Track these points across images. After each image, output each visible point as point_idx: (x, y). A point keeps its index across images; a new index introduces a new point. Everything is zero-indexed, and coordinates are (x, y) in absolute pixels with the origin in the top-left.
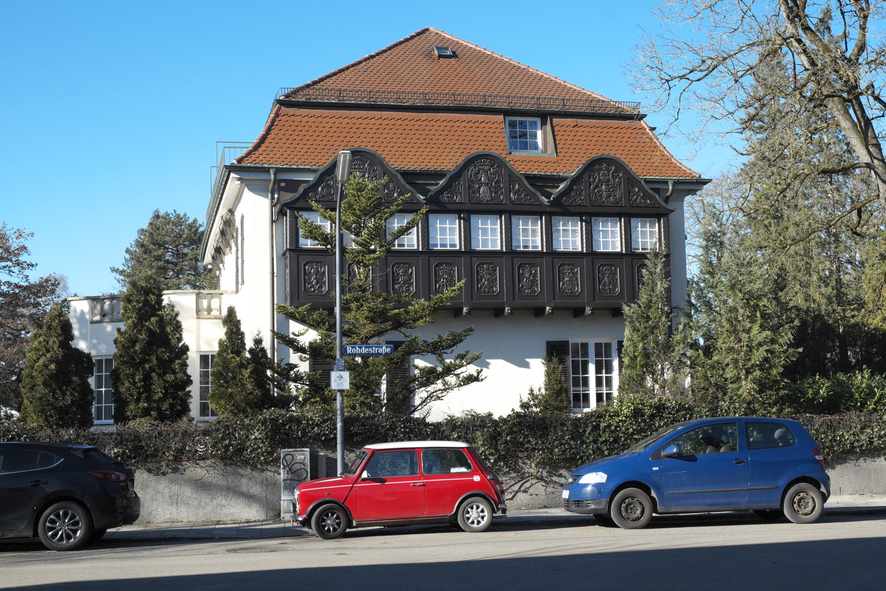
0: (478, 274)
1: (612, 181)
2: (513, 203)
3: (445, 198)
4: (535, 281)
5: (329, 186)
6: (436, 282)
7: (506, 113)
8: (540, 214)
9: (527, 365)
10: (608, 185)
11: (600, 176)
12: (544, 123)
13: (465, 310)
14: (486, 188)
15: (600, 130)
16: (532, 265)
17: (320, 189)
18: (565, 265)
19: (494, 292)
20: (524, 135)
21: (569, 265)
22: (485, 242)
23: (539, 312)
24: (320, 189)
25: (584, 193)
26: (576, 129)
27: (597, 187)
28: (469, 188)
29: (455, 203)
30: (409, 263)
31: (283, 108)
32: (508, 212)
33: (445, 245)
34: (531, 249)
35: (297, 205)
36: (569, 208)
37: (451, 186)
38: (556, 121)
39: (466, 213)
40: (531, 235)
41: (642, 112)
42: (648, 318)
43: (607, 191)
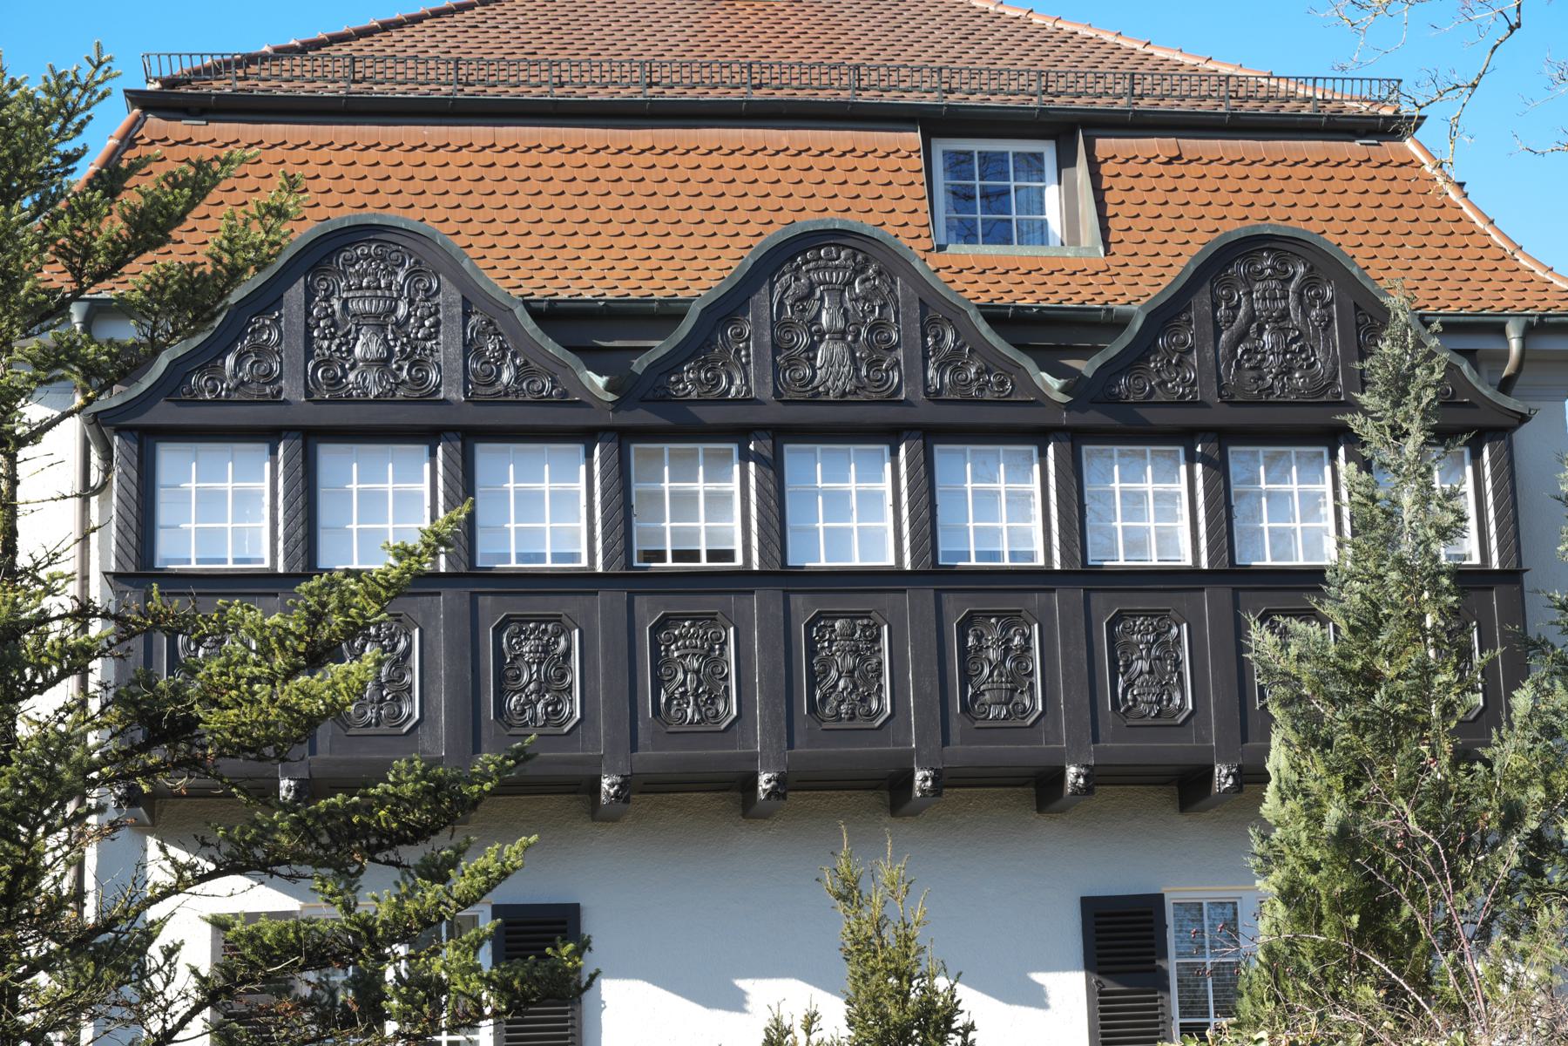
0: (812, 651)
1: (1295, 316)
2: (936, 398)
3: (688, 382)
4: (1030, 673)
5: (261, 350)
6: (658, 684)
7: (935, 123)
8: (1037, 436)
9: (1036, 998)
10: (1285, 331)
11: (1251, 299)
12: (1066, 160)
13: (764, 781)
14: (838, 348)
15: (1260, 170)
16: (1011, 619)
17: (230, 361)
18: (1134, 614)
19: (871, 716)
20: (995, 198)
21: (1147, 614)
22: (838, 538)
23: (1044, 788)
24: (230, 361)
25: (1194, 358)
26: (1176, 169)
27: (1242, 336)
28: (776, 349)
29: (723, 400)
30: (556, 619)
31: (152, 120)
32: (920, 431)
33: (694, 555)
34: (1006, 562)
35: (147, 419)
36: (1144, 412)
37: (709, 343)
38: (1105, 146)
39: (770, 436)
40: (1003, 511)
41: (1406, 109)
42: (1371, 678)
43: (1275, 347)
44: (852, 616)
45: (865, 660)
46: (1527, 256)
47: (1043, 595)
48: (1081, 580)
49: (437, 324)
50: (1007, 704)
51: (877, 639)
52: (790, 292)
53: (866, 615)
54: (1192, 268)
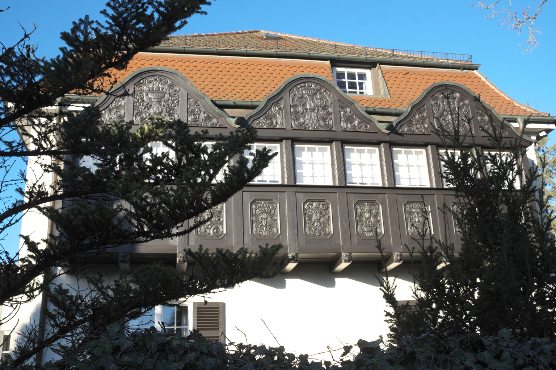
16: (373, 203)
46: (517, 103)
47: (382, 195)
49: (178, 102)
50: (372, 231)
51: (327, 209)
52: (296, 96)
53: (324, 201)
54: (425, 93)
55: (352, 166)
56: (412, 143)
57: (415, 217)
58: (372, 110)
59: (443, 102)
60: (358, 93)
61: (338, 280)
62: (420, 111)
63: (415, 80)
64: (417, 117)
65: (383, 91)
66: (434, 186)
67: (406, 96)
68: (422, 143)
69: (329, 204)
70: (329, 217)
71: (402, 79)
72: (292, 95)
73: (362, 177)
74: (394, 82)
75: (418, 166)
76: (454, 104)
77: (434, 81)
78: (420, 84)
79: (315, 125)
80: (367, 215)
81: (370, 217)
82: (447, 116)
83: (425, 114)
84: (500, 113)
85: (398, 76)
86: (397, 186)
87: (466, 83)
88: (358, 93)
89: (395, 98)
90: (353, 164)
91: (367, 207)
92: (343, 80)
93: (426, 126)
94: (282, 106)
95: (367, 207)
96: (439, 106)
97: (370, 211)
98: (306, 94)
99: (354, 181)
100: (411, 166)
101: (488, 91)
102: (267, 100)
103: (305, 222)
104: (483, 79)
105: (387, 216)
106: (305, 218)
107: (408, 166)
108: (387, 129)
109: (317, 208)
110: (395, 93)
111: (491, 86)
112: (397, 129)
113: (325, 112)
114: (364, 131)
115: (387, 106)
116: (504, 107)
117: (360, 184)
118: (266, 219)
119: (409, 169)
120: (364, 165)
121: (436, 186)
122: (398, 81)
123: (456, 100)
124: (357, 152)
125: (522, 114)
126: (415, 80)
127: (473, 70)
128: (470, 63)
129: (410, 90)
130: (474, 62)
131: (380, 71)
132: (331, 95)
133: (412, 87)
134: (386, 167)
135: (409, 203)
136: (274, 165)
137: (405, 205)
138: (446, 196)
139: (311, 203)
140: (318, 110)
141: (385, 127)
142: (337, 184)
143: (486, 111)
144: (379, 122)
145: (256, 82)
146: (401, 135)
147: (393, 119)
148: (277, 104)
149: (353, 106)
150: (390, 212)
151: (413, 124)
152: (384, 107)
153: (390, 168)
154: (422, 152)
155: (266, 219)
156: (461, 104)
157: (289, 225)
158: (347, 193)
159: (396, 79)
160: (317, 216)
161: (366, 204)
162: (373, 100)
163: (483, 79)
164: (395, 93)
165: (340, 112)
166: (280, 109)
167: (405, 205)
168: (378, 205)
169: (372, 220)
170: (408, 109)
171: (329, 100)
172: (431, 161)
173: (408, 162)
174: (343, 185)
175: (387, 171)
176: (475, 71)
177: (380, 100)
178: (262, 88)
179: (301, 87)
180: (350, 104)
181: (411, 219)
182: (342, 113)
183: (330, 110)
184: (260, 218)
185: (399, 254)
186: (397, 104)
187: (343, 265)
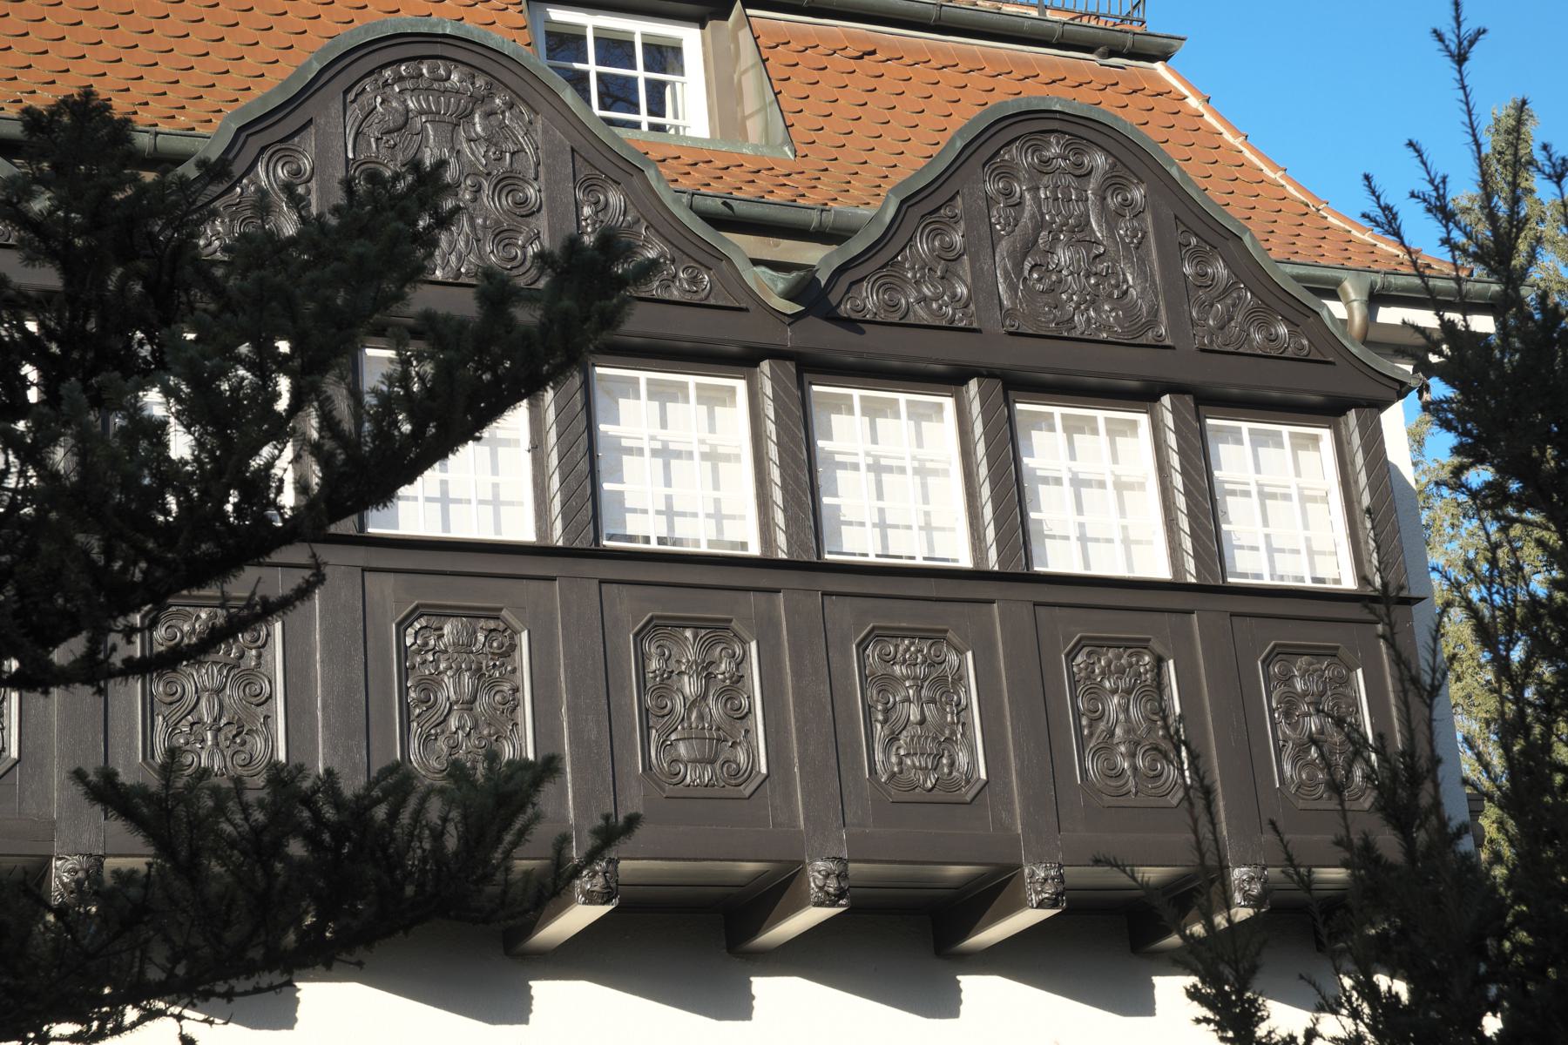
16: (716, 630)
44: (474, 614)
45: (493, 684)
46: (1337, 215)
47: (762, 597)
48: (800, 572)
50: (712, 762)
51: (511, 650)
52: (374, 119)
55: (840, 474)
56: (896, 363)
57: (907, 700)
58: (716, 205)
59: (1035, 190)
60: (645, 127)
61: (544, 991)
62: (936, 222)
63: (902, 86)
64: (922, 247)
65: (758, 131)
66: (993, 563)
67: (864, 156)
68: (939, 368)
69: (516, 632)
70: (516, 690)
71: (846, 79)
72: (355, 112)
73: (669, 513)
74: (807, 90)
75: (922, 472)
76: (1083, 199)
77: (985, 97)
78: (922, 104)
79: (460, 259)
80: (690, 686)
81: (704, 697)
82: (1051, 252)
83: (958, 239)
84: (1282, 252)
85: (825, 61)
86: (1037, 569)
87: (1146, 116)
88: (645, 127)
89: (816, 159)
90: (630, 451)
91: (689, 647)
92: (577, 66)
93: (961, 290)
94: (307, 165)
95: (689, 647)
96: (1020, 204)
97: (706, 671)
98: (421, 113)
99: (634, 525)
100: (890, 469)
101: (1215, 155)
102: (234, 127)
103: (406, 710)
104: (1193, 102)
105: (783, 693)
106: (404, 691)
107: (877, 468)
108: (789, 295)
109: (464, 647)
110: (814, 136)
111: (1228, 136)
112: (834, 298)
113: (507, 202)
114: (687, 298)
115: (781, 195)
116: (1284, 227)
117: (661, 541)
118: (219, 691)
119: (924, 486)
120: (678, 455)
121: (1000, 561)
122: (827, 86)
123: (1093, 184)
124: (652, 396)
125: (1357, 261)
126: (902, 86)
127: (1152, 58)
128: (1136, 27)
129: (880, 129)
130: (1157, 23)
131: (745, 36)
132: (539, 126)
133: (888, 115)
134: (781, 467)
135: (879, 635)
136: (494, 455)
137: (863, 647)
138: (1041, 611)
139: (435, 622)
140: (478, 189)
141: (781, 286)
142: (557, 538)
143: (1216, 236)
144: (756, 262)
145: (173, 43)
146: (850, 324)
147: (812, 254)
148: (283, 148)
149: (636, 181)
150: (797, 675)
151: (904, 280)
152: (769, 198)
153: (796, 473)
154: (1134, 423)
155: (219, 691)
156: (1113, 202)
157: (326, 726)
158: (602, 582)
159: (817, 75)
160: (458, 684)
161: (688, 633)
162: (686, 159)
163: (1193, 102)
164: (814, 136)
165: (578, 207)
166: (297, 173)
167: (863, 647)
168: (744, 642)
169: (715, 708)
170: (883, 209)
171: (529, 150)
172: (981, 449)
173: (663, 435)
174: (583, 543)
175: (784, 488)
176: (1159, 66)
177: (749, 166)
178: (202, 73)
179: (400, 79)
180: (627, 169)
181: (886, 711)
182: (587, 211)
183: (531, 192)
184: (190, 688)
185: (831, 865)
186: (826, 189)
187: (578, 917)
